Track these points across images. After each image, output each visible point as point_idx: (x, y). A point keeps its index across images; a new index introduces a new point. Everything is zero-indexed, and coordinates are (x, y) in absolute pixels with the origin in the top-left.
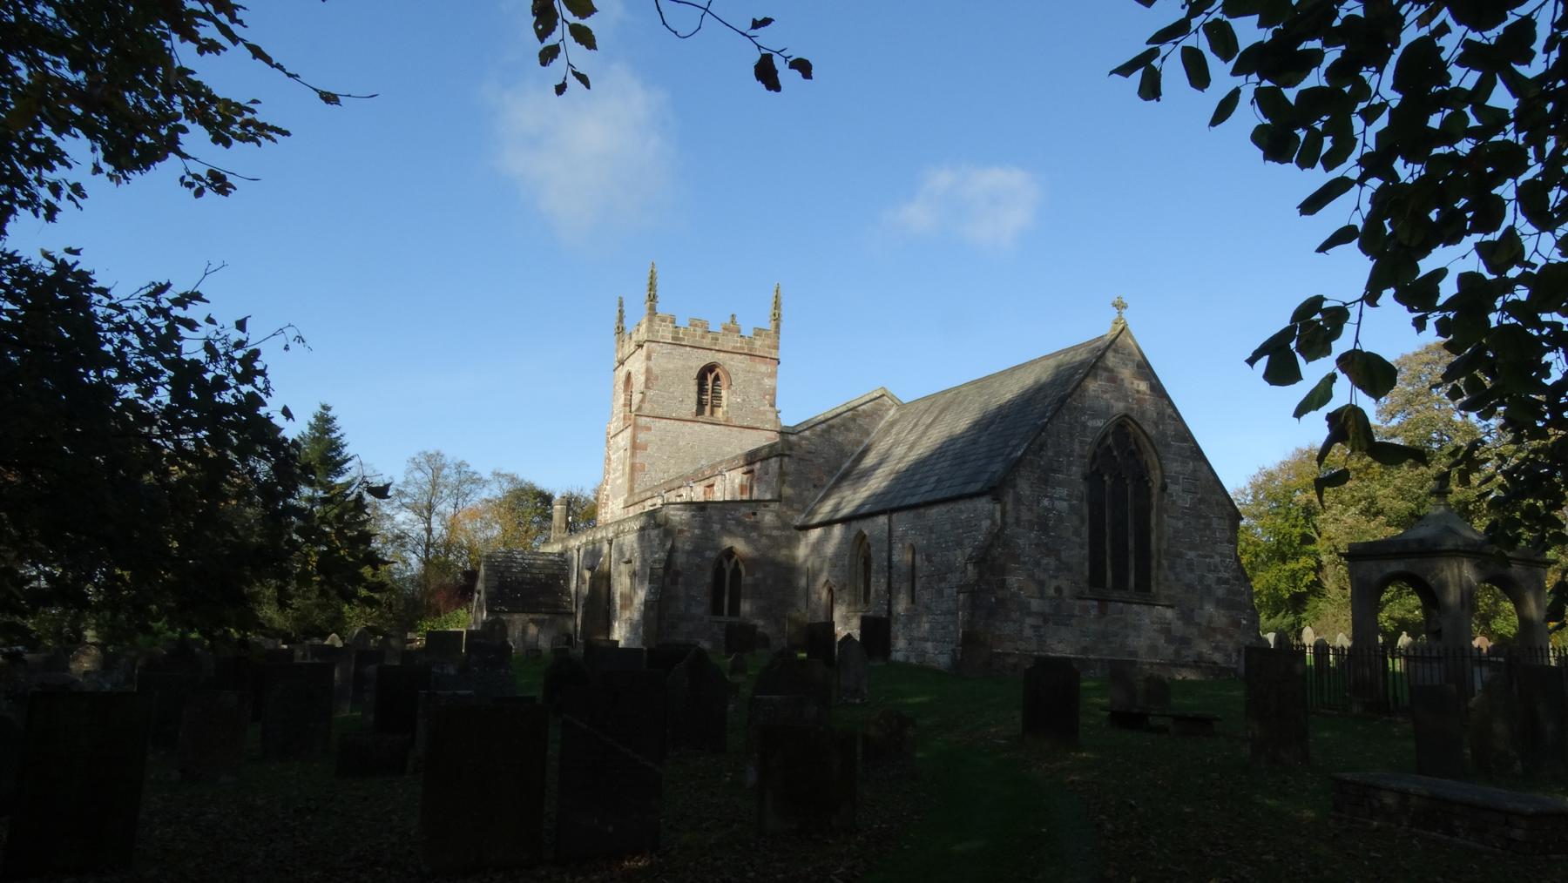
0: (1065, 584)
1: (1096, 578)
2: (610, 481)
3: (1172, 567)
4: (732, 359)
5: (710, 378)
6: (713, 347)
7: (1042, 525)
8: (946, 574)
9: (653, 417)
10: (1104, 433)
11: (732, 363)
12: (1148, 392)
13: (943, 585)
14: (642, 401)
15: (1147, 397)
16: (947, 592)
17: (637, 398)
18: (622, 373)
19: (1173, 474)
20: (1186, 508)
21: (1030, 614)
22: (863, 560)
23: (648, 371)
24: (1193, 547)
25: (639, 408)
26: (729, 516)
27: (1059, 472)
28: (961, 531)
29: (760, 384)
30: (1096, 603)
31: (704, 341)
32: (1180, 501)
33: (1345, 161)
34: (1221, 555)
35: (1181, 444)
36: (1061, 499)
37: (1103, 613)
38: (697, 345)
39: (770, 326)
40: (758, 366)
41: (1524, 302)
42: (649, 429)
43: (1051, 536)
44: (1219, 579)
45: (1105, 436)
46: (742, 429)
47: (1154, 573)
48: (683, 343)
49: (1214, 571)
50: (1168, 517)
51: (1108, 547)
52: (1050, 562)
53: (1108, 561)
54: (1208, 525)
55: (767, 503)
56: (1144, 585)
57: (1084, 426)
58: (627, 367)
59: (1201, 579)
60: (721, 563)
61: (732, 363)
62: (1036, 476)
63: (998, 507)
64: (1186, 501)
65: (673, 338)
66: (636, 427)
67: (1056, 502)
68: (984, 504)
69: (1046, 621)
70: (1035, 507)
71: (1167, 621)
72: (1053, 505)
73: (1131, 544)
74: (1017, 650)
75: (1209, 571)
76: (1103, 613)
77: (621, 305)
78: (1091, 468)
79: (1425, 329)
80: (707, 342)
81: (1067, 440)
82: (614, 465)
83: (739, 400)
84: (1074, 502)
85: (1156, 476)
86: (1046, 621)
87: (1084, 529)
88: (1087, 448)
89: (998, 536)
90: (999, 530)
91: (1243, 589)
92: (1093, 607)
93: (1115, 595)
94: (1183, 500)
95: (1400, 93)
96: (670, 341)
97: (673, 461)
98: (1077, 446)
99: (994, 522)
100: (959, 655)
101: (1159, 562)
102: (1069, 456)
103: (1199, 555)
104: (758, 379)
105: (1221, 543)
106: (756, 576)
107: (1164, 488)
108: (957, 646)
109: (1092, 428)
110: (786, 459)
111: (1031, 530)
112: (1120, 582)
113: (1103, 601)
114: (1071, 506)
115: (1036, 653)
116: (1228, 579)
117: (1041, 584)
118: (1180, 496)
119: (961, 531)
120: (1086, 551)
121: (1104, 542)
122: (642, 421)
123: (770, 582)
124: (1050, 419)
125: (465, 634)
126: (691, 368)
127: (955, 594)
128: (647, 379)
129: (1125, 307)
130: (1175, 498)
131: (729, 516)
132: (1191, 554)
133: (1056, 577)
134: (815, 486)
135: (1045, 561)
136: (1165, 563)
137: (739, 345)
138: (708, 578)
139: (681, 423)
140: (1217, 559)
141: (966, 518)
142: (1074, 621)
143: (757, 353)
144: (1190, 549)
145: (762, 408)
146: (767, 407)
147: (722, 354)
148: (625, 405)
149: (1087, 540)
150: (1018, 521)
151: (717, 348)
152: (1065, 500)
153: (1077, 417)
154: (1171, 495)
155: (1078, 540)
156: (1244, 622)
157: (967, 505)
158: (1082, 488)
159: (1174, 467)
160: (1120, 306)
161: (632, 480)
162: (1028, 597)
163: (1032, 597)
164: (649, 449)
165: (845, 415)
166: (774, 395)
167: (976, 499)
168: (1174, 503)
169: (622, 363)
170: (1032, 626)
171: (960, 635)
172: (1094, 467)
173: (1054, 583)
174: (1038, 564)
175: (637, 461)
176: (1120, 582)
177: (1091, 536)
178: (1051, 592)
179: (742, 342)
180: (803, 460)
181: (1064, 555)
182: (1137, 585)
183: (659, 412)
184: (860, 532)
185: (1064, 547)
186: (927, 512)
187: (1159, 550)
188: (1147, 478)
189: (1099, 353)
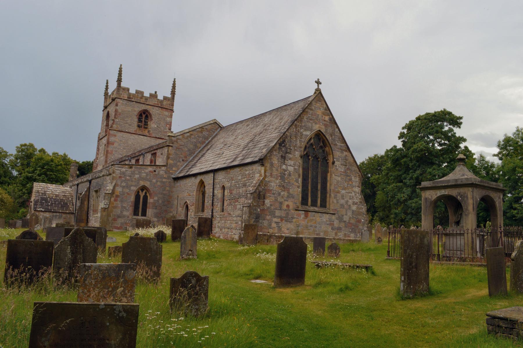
0: (291, 204)
1: (304, 201)
2: (98, 158)
3: (335, 197)
4: (153, 109)
5: (144, 116)
6: (145, 103)
7: (282, 177)
8: (238, 199)
9: (117, 131)
10: (310, 138)
11: (153, 110)
12: (329, 121)
13: (237, 203)
14: (113, 124)
15: (328, 123)
16: (238, 207)
19: (337, 157)
20: (342, 172)
21: (275, 217)
22: (202, 193)
23: (116, 111)
24: (344, 189)
25: (112, 127)
26: (143, 172)
27: (290, 153)
28: (246, 179)
29: (164, 120)
30: (303, 212)
31: (141, 100)
32: (340, 169)
34: (355, 192)
35: (341, 145)
36: (290, 165)
37: (306, 216)
38: (138, 101)
39: (169, 96)
40: (164, 112)
42: (115, 136)
43: (286, 182)
44: (354, 202)
45: (310, 139)
46: (156, 139)
47: (328, 199)
48: (132, 100)
49: (352, 199)
50: (335, 175)
51: (310, 188)
52: (285, 194)
53: (309, 195)
54: (350, 180)
55: (161, 167)
56: (324, 205)
57: (302, 134)
58: (108, 109)
59: (347, 202)
60: (138, 192)
61: (153, 110)
62: (280, 155)
63: (263, 168)
65: (128, 98)
67: (288, 167)
68: (257, 167)
69: (282, 220)
70: (279, 169)
71: (333, 220)
72: (287, 168)
74: (269, 233)
75: (350, 199)
76: (306, 216)
77: (107, 83)
78: (304, 153)
80: (143, 101)
81: (294, 140)
82: (100, 151)
83: (155, 126)
84: (296, 167)
86: (282, 220)
87: (300, 179)
88: (303, 144)
89: (262, 183)
90: (263, 178)
91: (363, 207)
92: (303, 214)
93: (312, 208)
94: (341, 168)
96: (127, 99)
97: (125, 150)
98: (298, 142)
99: (261, 175)
100: (242, 235)
101: (330, 195)
102: (295, 147)
103: (346, 192)
104: (164, 118)
105: (355, 187)
106: (155, 199)
107: (333, 163)
108: (242, 231)
109: (305, 135)
110: (170, 148)
111: (277, 179)
113: (306, 211)
114: (295, 169)
115: (277, 234)
116: (357, 203)
117: (281, 203)
119: (246, 179)
120: (300, 190)
121: (308, 186)
122: (111, 132)
123: (160, 202)
125: (140, 214)
126: (135, 111)
127: (242, 208)
128: (115, 115)
129: (321, 84)
130: (338, 167)
131: (143, 172)
133: (287, 201)
134: (183, 160)
135: (282, 193)
136: (332, 195)
137: (157, 103)
138: (132, 198)
139: (129, 134)
140: (353, 194)
141: (248, 173)
142: (294, 220)
143: (164, 107)
144: (343, 189)
145: (165, 130)
146: (168, 130)
147: (149, 106)
148: (106, 126)
149: (301, 184)
150: (271, 175)
151: (147, 103)
152: (293, 166)
153: (299, 130)
154: (336, 166)
155: (297, 184)
156: (363, 220)
157: (249, 167)
158: (300, 161)
160: (318, 82)
161: (107, 157)
162: (274, 209)
163: (277, 209)
164: (115, 144)
165: (198, 130)
166: (170, 125)
167: (253, 165)
168: (337, 169)
170: (276, 222)
171: (243, 226)
172: (305, 153)
174: (279, 194)
175: (109, 149)
177: (303, 183)
178: (285, 207)
179: (158, 102)
180: (178, 148)
181: (291, 191)
182: (321, 205)
183: (120, 129)
184: (201, 180)
185: (291, 187)
186: (231, 171)
187: (330, 190)
188: (327, 159)
189: (309, 103)
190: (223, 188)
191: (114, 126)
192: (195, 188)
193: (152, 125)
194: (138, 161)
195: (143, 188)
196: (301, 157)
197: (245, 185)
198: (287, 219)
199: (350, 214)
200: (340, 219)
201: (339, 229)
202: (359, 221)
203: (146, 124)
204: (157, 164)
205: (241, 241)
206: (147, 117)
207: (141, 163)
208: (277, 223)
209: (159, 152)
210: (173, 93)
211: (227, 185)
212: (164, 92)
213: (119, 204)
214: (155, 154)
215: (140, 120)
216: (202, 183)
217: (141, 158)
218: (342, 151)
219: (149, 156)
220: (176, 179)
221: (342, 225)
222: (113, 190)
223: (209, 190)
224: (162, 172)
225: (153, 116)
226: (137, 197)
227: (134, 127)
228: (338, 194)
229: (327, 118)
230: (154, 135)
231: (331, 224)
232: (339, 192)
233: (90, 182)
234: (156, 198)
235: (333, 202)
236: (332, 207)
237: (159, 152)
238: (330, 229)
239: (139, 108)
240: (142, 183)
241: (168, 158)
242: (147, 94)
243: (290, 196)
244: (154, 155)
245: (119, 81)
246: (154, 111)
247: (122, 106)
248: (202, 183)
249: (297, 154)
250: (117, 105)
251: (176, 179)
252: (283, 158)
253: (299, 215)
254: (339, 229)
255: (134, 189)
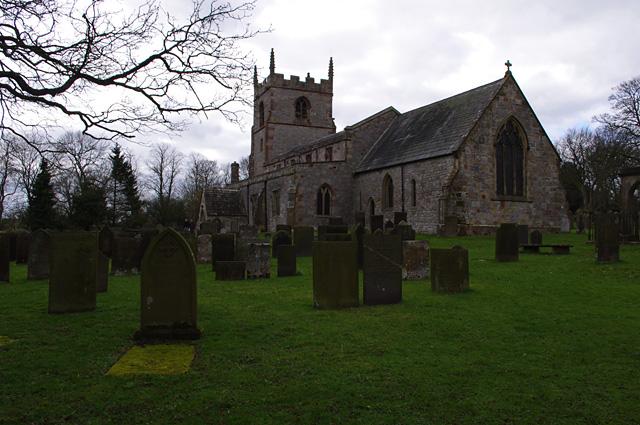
1: (500, 191)
7: (476, 168)
17: (266, 114)
23: (272, 101)
39: (327, 78)
56: (520, 193)
64: (538, 154)
66: (268, 129)
68: (449, 160)
73: (515, 175)
76: (503, 206)
89: (456, 176)
107: (528, 149)
112: (510, 192)
113: (502, 201)
118: (535, 152)
122: (270, 125)
124: (479, 119)
132: (540, 178)
138: (315, 197)
159: (532, 139)
160: (508, 64)
161: (267, 154)
176: (510, 192)
190: (414, 182)
191: (272, 119)
193: (312, 114)
194: (309, 157)
195: (325, 186)
196: (495, 145)
197: (438, 178)
201: (537, 217)
203: (305, 113)
204: (334, 159)
205: (29, 279)
206: (304, 105)
207: (314, 160)
210: (331, 73)
212: (320, 75)
213: (302, 203)
214: (331, 148)
215: (298, 110)
217: (314, 155)
218: (534, 126)
219: (323, 152)
220: (357, 175)
222: (297, 190)
223: (397, 184)
224: (342, 169)
226: (320, 195)
227: (292, 118)
228: (535, 182)
230: (313, 124)
231: (529, 213)
232: (535, 179)
233: (266, 182)
234: (338, 196)
237: (335, 147)
238: (527, 218)
240: (323, 181)
241: (347, 153)
243: (486, 186)
244: (330, 150)
245: (272, 67)
246: (312, 97)
247: (279, 96)
250: (272, 95)
251: (357, 175)
253: (496, 206)
254: (537, 217)
255: (316, 187)
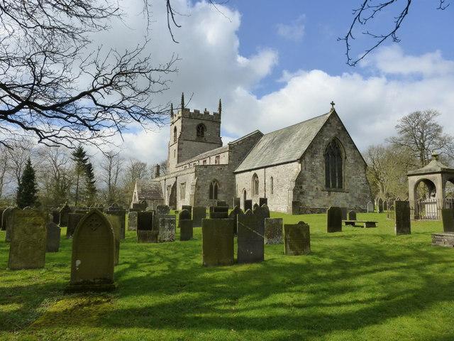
0: (318, 186)
1: (327, 185)
18: (173, 126)
33: (331, 76)
37: (329, 195)
39: (218, 112)
41: (242, 19)
56: (341, 186)
76: (329, 195)
79: (237, 33)
80: (199, 117)
85: (343, 154)
95: (232, 8)
107: (346, 158)
112: (334, 186)
113: (329, 192)
132: (354, 177)
136: (346, 180)
160: (333, 104)
169: (173, 123)
173: (316, 187)
176: (334, 186)
192: (251, 178)
193: (207, 134)
198: (317, 197)
199: (359, 192)
200: (352, 196)
201: (352, 202)
202: (366, 197)
208: (311, 200)
209: (221, 155)
211: (275, 176)
215: (198, 131)
216: (255, 176)
221: (354, 199)
225: (207, 128)
226: (211, 187)
227: (194, 137)
229: (340, 128)
230: (208, 141)
231: (347, 199)
233: (176, 178)
235: (346, 186)
236: (346, 188)
237: (221, 155)
239: (197, 123)
240: (214, 177)
242: (202, 112)
246: (208, 124)
248: (255, 176)
249: (322, 154)
252: (312, 157)
